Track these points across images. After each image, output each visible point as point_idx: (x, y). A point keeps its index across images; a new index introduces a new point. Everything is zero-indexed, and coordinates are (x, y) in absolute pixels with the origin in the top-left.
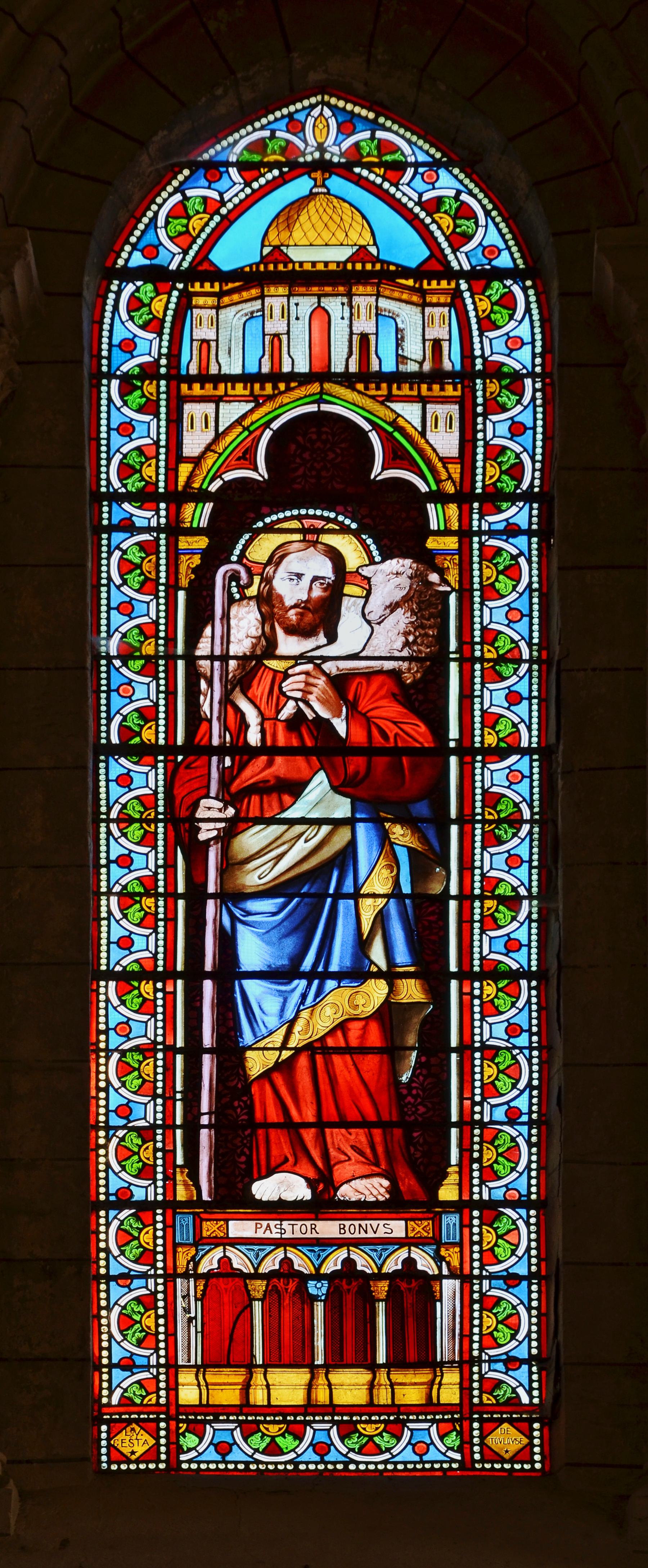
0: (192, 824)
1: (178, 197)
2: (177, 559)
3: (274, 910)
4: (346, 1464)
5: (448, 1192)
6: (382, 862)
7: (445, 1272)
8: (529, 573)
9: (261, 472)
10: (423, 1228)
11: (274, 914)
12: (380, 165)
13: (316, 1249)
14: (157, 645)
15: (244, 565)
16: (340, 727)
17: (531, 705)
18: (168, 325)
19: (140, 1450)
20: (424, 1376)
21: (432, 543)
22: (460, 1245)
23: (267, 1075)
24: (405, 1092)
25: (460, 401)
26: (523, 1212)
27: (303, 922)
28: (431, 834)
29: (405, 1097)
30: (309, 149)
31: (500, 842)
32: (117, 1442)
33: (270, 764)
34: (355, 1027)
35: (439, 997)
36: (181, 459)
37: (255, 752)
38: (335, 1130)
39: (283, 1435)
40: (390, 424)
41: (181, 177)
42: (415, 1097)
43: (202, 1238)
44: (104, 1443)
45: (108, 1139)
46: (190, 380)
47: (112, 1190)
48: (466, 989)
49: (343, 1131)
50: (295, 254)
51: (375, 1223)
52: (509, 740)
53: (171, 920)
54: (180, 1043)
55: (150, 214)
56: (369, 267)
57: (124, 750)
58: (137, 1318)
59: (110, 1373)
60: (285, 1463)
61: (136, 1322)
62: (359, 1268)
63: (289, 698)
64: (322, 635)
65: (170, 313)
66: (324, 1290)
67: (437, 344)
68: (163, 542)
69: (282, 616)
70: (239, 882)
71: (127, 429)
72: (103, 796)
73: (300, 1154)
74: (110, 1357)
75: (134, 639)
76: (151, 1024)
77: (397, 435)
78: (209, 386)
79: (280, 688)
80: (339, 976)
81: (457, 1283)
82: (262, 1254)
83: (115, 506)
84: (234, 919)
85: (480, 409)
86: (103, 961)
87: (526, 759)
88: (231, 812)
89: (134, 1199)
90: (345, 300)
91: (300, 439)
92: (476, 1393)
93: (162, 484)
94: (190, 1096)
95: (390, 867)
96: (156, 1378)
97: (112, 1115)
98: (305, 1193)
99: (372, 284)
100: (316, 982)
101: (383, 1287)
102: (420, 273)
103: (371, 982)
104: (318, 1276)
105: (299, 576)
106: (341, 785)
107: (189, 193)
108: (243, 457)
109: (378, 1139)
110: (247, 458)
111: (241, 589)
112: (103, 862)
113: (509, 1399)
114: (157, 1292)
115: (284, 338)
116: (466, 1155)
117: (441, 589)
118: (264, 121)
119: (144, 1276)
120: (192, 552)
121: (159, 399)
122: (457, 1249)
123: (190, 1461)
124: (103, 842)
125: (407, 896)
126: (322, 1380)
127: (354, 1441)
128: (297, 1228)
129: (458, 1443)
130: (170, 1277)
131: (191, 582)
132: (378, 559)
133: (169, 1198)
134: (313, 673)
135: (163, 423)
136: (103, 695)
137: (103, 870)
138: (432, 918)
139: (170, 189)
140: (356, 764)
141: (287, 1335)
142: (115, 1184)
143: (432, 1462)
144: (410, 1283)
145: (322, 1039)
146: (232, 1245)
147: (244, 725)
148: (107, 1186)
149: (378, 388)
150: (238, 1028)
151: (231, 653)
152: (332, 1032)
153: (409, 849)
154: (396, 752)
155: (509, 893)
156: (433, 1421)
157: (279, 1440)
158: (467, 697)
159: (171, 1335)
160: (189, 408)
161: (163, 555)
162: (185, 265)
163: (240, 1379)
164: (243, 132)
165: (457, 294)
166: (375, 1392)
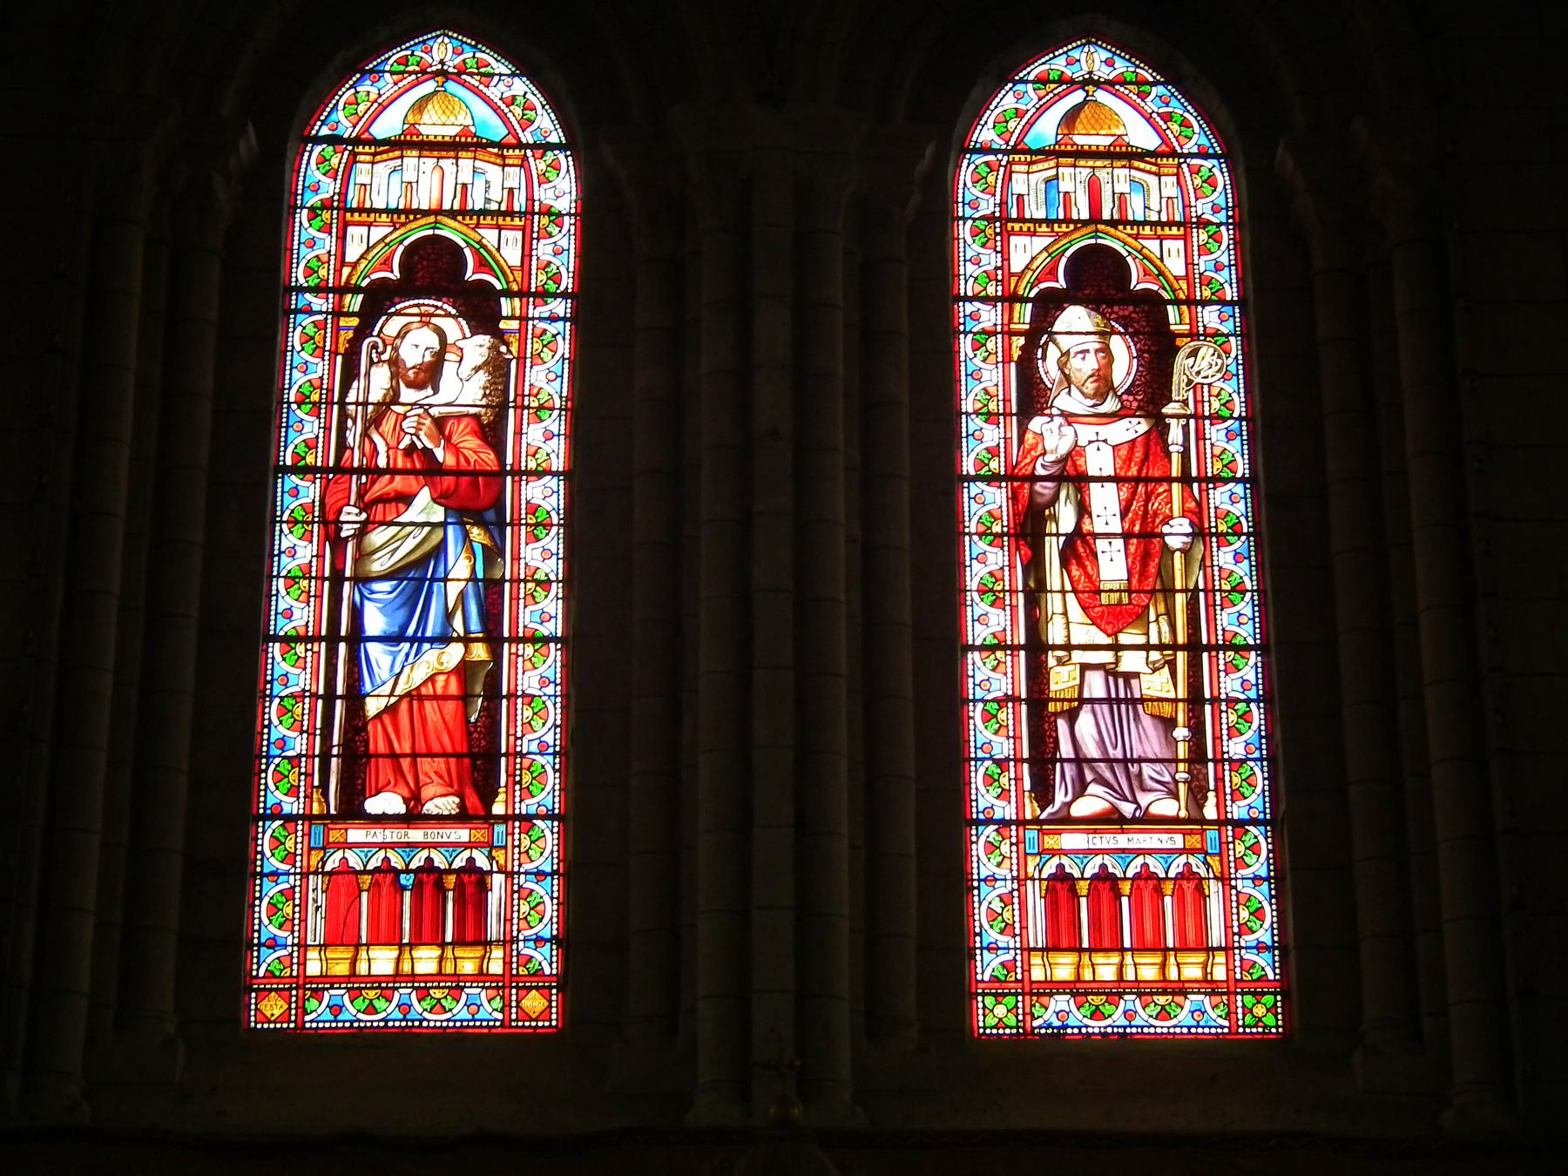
0: (338, 525)
1: (353, 91)
2: (338, 333)
3: (389, 590)
4: (421, 1021)
5: (498, 808)
6: (464, 555)
7: (495, 869)
8: (564, 347)
9: (396, 274)
10: (1194, 841)
11: (390, 593)
12: (477, 74)
13: (408, 850)
14: (321, 394)
15: (381, 338)
16: (439, 454)
17: (1230, 270)
18: (340, 173)
19: (277, 1013)
20: (477, 952)
21: (503, 325)
22: (505, 848)
23: (379, 716)
24: (472, 729)
25: (523, 229)
26: (549, 823)
27: (408, 599)
28: (496, 534)
29: (472, 733)
30: (435, 63)
31: (537, 539)
32: (261, 1006)
33: (391, 481)
34: (441, 679)
35: (496, 656)
36: (343, 263)
37: (382, 472)
38: (424, 759)
39: (378, 998)
40: (477, 243)
41: (354, 79)
42: (479, 733)
43: (329, 843)
44: (253, 1007)
45: (268, 765)
46: (352, 211)
47: (269, 805)
48: (514, 650)
49: (429, 759)
50: (423, 130)
51: (448, 831)
52: (543, 465)
53: (319, 596)
54: (321, 692)
55: (334, 102)
56: (469, 140)
57: (294, 470)
58: (280, 906)
59: (259, 951)
60: (379, 1021)
61: (279, 910)
62: (436, 864)
63: (407, 433)
64: (430, 388)
65: (342, 165)
66: (411, 881)
67: (511, 191)
68: (329, 321)
69: (404, 375)
70: (368, 568)
71: (312, 243)
72: (279, 503)
73: (399, 778)
74: (259, 938)
75: (306, 390)
76: (302, 676)
77: (482, 251)
78: (364, 215)
79: (401, 425)
80: (432, 640)
81: (503, 876)
82: (369, 855)
83: (300, 296)
84: (362, 596)
85: (535, 235)
86: (272, 628)
87: (556, 479)
88: (364, 516)
89: (284, 812)
90: (454, 161)
91: (421, 252)
92: (514, 966)
93: (331, 281)
94: (326, 732)
95: (469, 558)
96: (291, 955)
97: (272, 746)
98: (402, 809)
99: (471, 151)
100: (416, 645)
101: (452, 879)
102: (1155, 154)
103: (453, 645)
104: (407, 871)
105: (417, 346)
106: (439, 497)
107: (359, 89)
108: (1050, 273)
109: (453, 767)
110: (387, 264)
111: (379, 354)
112: (276, 552)
113: (537, 971)
114: (295, 886)
115: (414, 185)
116: (511, 779)
117: (508, 357)
118: (408, 45)
119: (287, 874)
120: (348, 328)
121: (331, 223)
122: (503, 851)
123: (311, 1021)
124: (277, 537)
125: (480, 580)
126: (407, 955)
127: (427, 1004)
128: (395, 835)
129: (501, 1005)
130: (305, 875)
131: (346, 349)
132: (468, 334)
133: (307, 812)
134: (423, 415)
135: (334, 239)
136: (283, 430)
137: (276, 559)
138: (495, 596)
139: (347, 86)
140: (449, 481)
141: (383, 920)
142: (271, 801)
143: (482, 1020)
144: (470, 877)
145: (418, 688)
146: (350, 848)
147: (375, 452)
148: (265, 802)
149: (471, 219)
150: (361, 679)
151: (370, 401)
152: (425, 683)
153: (483, 544)
154: (475, 474)
155: (543, 578)
156: (483, 987)
157: (376, 1003)
158: (519, 433)
159: (304, 920)
160: (351, 230)
161: (329, 330)
162: (354, 135)
163: (349, 955)
164: (395, 51)
165: (525, 158)
166: (443, 964)
